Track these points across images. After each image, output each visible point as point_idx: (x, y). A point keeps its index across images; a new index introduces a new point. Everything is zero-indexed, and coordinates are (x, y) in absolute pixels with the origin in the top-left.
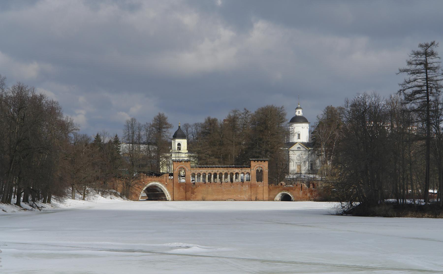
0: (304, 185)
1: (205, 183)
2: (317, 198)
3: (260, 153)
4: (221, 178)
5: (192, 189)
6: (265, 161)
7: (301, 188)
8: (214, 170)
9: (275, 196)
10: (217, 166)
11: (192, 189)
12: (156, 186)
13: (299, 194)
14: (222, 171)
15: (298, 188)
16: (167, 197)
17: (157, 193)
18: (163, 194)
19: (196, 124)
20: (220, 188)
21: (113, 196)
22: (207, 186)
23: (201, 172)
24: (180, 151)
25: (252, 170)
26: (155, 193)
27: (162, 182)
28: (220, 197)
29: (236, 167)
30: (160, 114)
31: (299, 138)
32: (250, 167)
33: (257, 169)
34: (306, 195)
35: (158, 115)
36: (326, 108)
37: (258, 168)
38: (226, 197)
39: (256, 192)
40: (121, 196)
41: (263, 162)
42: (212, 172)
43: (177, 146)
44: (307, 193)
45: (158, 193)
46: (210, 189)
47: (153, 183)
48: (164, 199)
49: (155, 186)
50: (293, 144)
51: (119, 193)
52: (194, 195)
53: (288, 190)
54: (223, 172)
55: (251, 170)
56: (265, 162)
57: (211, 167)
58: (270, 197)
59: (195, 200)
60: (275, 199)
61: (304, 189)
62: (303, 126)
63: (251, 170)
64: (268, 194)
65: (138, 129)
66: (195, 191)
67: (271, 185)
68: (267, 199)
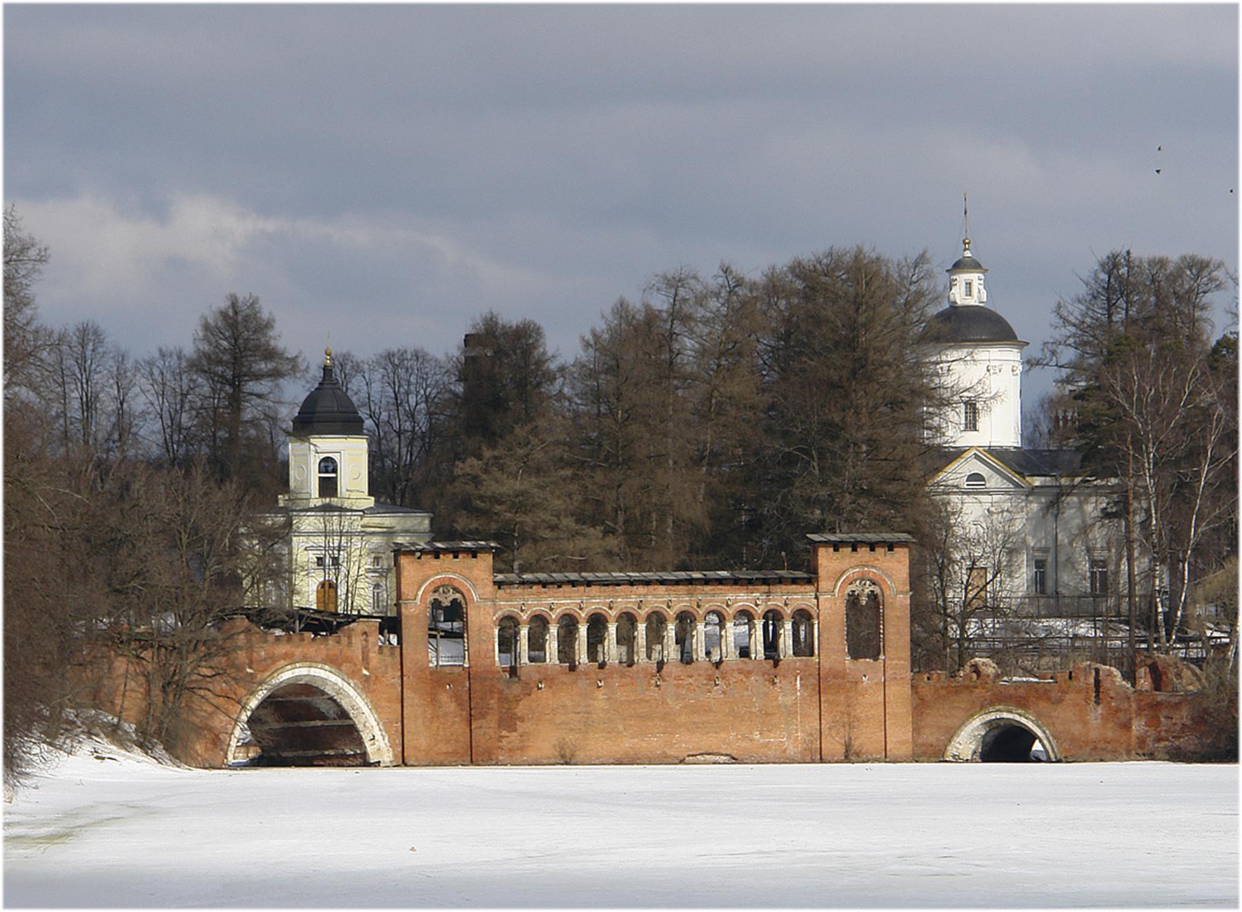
0: (1110, 674)
1: (573, 668)
2: (1183, 742)
3: (830, 505)
4: (626, 639)
5: (503, 699)
6: (891, 547)
7: (1097, 691)
8: (618, 597)
9: (951, 733)
10: (638, 574)
11: (503, 699)
12: (311, 686)
13: (1085, 723)
14: (662, 602)
15: (1079, 692)
16: (370, 749)
17: (312, 723)
18: (350, 732)
19: (389, 356)
20: (653, 693)
21: (106, 746)
22: (582, 683)
23: (551, 609)
24: (334, 501)
25: (821, 598)
26: (303, 724)
27: (343, 668)
28: (654, 743)
29: (736, 582)
30: (234, 305)
31: (972, 425)
32: (811, 579)
33: (852, 587)
34: (1126, 726)
35: (224, 304)
36: (1102, 265)
37: (856, 587)
38: (683, 742)
39: (849, 715)
40: (141, 746)
41: (880, 551)
42: (611, 608)
43: (314, 477)
44: (1130, 719)
45: (319, 723)
46: (600, 700)
47: (297, 672)
48: (355, 756)
49: (309, 689)
50: (954, 455)
51: (130, 727)
52: (515, 734)
53: (1021, 701)
54: (669, 607)
55: (817, 598)
56: (891, 549)
57: (605, 583)
58: (920, 741)
59: (519, 761)
60: (951, 750)
61: (1112, 694)
62: (993, 363)
63: (817, 598)
64: (913, 723)
65: (111, 381)
66: (521, 709)
67: (929, 679)
68: (907, 750)
